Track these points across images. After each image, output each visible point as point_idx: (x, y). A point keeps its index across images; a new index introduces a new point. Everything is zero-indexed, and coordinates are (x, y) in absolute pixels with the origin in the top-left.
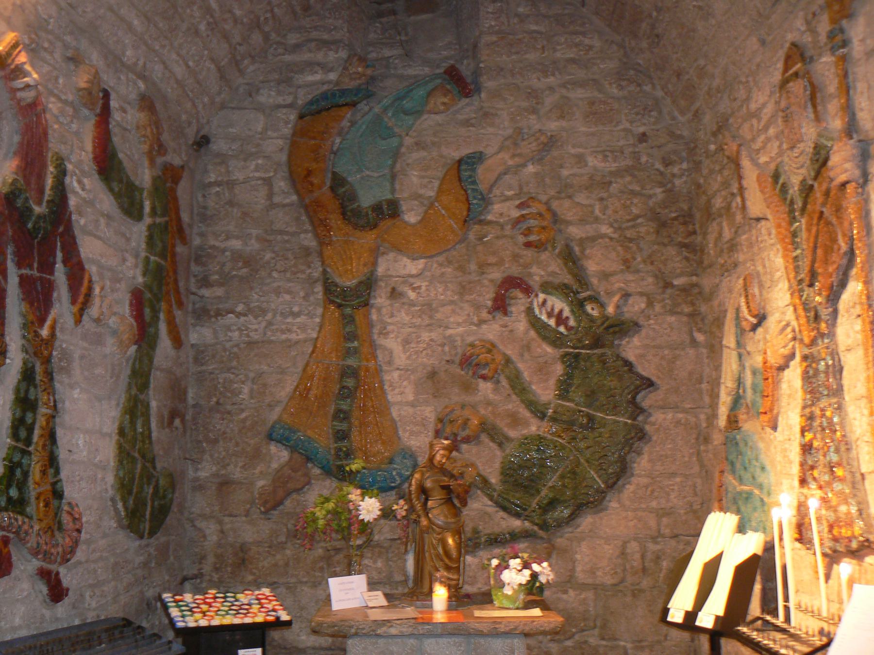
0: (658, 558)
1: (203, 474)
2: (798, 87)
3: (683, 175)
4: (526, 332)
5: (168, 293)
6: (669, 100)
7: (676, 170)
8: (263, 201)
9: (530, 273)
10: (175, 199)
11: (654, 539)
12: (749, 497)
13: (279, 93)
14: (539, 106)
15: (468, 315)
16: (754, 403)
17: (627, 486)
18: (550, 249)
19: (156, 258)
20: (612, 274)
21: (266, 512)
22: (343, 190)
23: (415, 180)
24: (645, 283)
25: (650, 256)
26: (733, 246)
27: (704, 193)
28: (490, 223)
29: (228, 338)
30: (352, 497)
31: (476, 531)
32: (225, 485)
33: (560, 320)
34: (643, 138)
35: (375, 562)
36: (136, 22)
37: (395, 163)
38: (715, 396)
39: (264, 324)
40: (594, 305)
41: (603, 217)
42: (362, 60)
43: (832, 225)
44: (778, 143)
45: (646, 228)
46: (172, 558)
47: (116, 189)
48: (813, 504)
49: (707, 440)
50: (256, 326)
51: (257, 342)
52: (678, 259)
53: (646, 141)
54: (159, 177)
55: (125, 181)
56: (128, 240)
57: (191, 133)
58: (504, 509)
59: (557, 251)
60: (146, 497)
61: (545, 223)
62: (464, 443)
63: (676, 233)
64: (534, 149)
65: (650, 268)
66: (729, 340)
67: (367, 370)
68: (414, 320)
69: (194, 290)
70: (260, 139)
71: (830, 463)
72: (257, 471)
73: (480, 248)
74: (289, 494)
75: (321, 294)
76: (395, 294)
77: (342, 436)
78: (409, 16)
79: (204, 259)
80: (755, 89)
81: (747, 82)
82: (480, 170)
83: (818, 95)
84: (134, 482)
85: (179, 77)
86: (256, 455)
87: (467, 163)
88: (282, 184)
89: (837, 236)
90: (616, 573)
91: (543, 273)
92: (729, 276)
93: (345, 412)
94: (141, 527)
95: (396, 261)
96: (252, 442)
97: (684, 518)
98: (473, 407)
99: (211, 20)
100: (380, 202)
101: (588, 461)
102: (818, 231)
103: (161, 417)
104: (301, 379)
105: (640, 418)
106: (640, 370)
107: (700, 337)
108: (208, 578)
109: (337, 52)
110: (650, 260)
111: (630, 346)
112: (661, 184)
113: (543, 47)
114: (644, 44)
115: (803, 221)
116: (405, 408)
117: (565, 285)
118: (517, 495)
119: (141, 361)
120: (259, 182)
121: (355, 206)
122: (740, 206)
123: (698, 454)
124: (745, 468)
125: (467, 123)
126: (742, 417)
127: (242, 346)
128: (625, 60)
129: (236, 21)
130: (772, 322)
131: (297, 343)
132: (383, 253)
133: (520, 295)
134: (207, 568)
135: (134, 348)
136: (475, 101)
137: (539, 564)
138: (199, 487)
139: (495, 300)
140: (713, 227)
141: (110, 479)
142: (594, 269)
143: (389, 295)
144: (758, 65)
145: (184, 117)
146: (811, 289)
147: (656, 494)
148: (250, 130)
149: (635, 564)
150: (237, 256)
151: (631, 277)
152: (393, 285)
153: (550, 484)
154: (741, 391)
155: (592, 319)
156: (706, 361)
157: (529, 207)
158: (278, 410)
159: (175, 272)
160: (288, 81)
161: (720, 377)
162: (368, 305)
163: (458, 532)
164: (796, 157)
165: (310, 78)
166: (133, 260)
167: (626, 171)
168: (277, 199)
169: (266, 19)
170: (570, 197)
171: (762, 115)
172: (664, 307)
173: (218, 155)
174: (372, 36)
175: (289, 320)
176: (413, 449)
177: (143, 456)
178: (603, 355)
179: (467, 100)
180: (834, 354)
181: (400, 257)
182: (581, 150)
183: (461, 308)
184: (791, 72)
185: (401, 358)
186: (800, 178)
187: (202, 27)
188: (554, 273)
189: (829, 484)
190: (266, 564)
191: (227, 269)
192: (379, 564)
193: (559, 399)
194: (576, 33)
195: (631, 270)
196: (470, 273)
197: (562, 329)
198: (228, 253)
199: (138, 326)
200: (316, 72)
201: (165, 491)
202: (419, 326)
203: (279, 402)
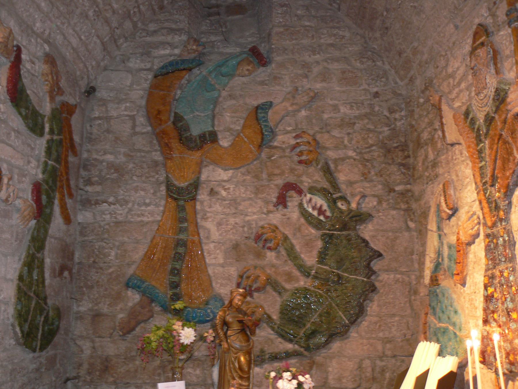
0: (383, 371)
1: (82, 309)
2: (481, 52)
3: (402, 119)
4: (298, 219)
5: (62, 187)
6: (393, 71)
7: (397, 116)
8: (129, 130)
9: (301, 181)
10: (70, 126)
11: (381, 358)
12: (445, 331)
13: (142, 61)
14: (309, 73)
15: (261, 207)
16: (449, 268)
17: (363, 322)
18: (315, 165)
19: (52, 163)
20: (356, 182)
21: (124, 335)
22: (181, 124)
23: (228, 119)
24: (376, 189)
25: (380, 172)
26: (435, 164)
27: (416, 130)
28: (276, 147)
29: (102, 219)
30: (176, 327)
31: (262, 351)
32: (97, 316)
33: (321, 212)
34: (376, 95)
35: (195, 371)
36: (43, 4)
37: (215, 107)
38: (422, 264)
39: (126, 210)
40: (343, 203)
41: (350, 145)
42: (195, 40)
43: (509, 143)
44: (468, 93)
45: (377, 152)
46: (58, 365)
47: (24, 113)
48: (496, 337)
49: (416, 292)
50: (121, 212)
51: (120, 222)
52: (398, 173)
53: (378, 97)
54: (57, 109)
55: (31, 108)
56: (33, 149)
57: (83, 84)
58: (282, 337)
59: (319, 166)
60: (38, 324)
61: (311, 149)
62: (256, 292)
63: (397, 156)
64: (305, 100)
65: (380, 179)
66: (432, 226)
67: (193, 242)
68: (225, 210)
69: (82, 187)
70: (129, 90)
71: (507, 309)
72: (118, 308)
73: (269, 164)
74: (138, 323)
75: (165, 191)
76: (212, 192)
77: (175, 285)
78: (228, 16)
79: (89, 167)
80: (452, 58)
81: (446, 54)
82: (270, 113)
83: (499, 57)
84: (29, 314)
85: (75, 46)
86: (118, 297)
87: (262, 109)
88: (142, 119)
89: (512, 150)
90: (355, 381)
91: (310, 181)
92: (433, 183)
93: (177, 270)
94: (34, 344)
95: (214, 171)
96: (116, 288)
97: (401, 344)
98: (263, 268)
99: (97, 9)
100: (205, 132)
101: (337, 305)
102: (497, 148)
103: (53, 270)
104: (150, 247)
105: (373, 277)
106: (372, 245)
107: (412, 225)
108: (83, 379)
109: (180, 36)
110: (380, 174)
111: (366, 230)
112: (388, 125)
113: (313, 36)
114: (378, 35)
115: (487, 142)
116: (218, 268)
117: (324, 188)
118: (291, 327)
119: (38, 231)
120: (127, 118)
121: (188, 134)
122: (441, 137)
123: (410, 301)
124: (443, 312)
125: (262, 83)
126: (441, 277)
127: (112, 224)
128: (365, 45)
129: (114, 12)
130: (463, 214)
131: (147, 223)
132: (206, 166)
133: (295, 195)
134: (82, 372)
135: (34, 222)
136: (269, 69)
137: (303, 376)
138: (80, 317)
139: (278, 198)
140: (422, 152)
141: (11, 310)
142: (343, 179)
143: (209, 193)
144: (454, 43)
145: (78, 73)
146: (493, 188)
147: (382, 328)
148: (122, 84)
149: (368, 375)
150: (111, 166)
151: (367, 185)
152: (212, 187)
153: (312, 320)
154: (440, 260)
155: (341, 212)
156: (416, 240)
157: (301, 137)
158: (134, 267)
159: (67, 173)
160: (148, 54)
161: (425, 251)
162: (195, 199)
163: (248, 353)
164: (481, 100)
165: (162, 52)
166: (36, 163)
167: (365, 116)
168: (138, 129)
169: (134, 12)
170: (328, 132)
171: (457, 75)
172: (388, 204)
173: (101, 100)
174: (204, 28)
175: (143, 208)
176: (223, 295)
177: (37, 296)
178: (349, 235)
179: (264, 69)
180: (509, 232)
181: (216, 169)
182: (336, 102)
183: (256, 203)
184: (478, 43)
185: (215, 235)
186: (485, 113)
187: (91, 13)
188: (316, 181)
189: (505, 323)
190: (122, 370)
191: (103, 174)
192: (198, 372)
193: (318, 264)
194: (334, 27)
195: (368, 180)
196: (262, 180)
197: (322, 218)
198: (104, 164)
199: (37, 208)
200: (167, 49)
201: (53, 319)
202: (228, 214)
203: (134, 262)
